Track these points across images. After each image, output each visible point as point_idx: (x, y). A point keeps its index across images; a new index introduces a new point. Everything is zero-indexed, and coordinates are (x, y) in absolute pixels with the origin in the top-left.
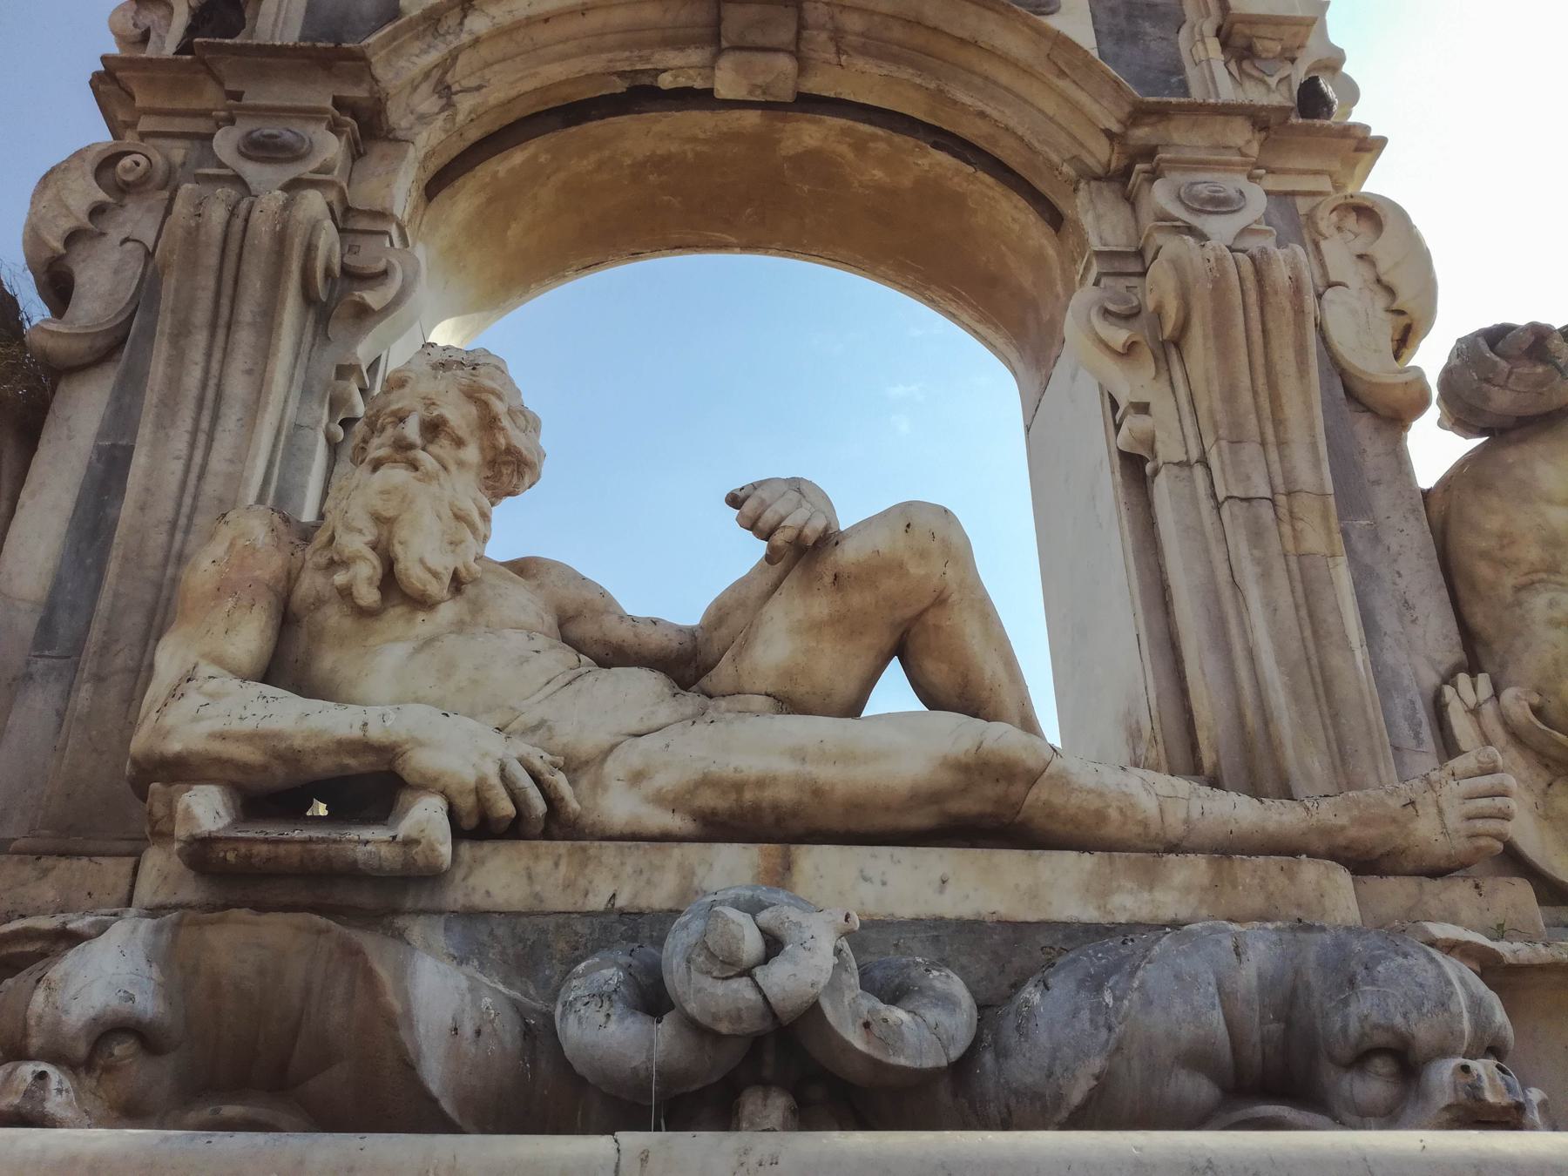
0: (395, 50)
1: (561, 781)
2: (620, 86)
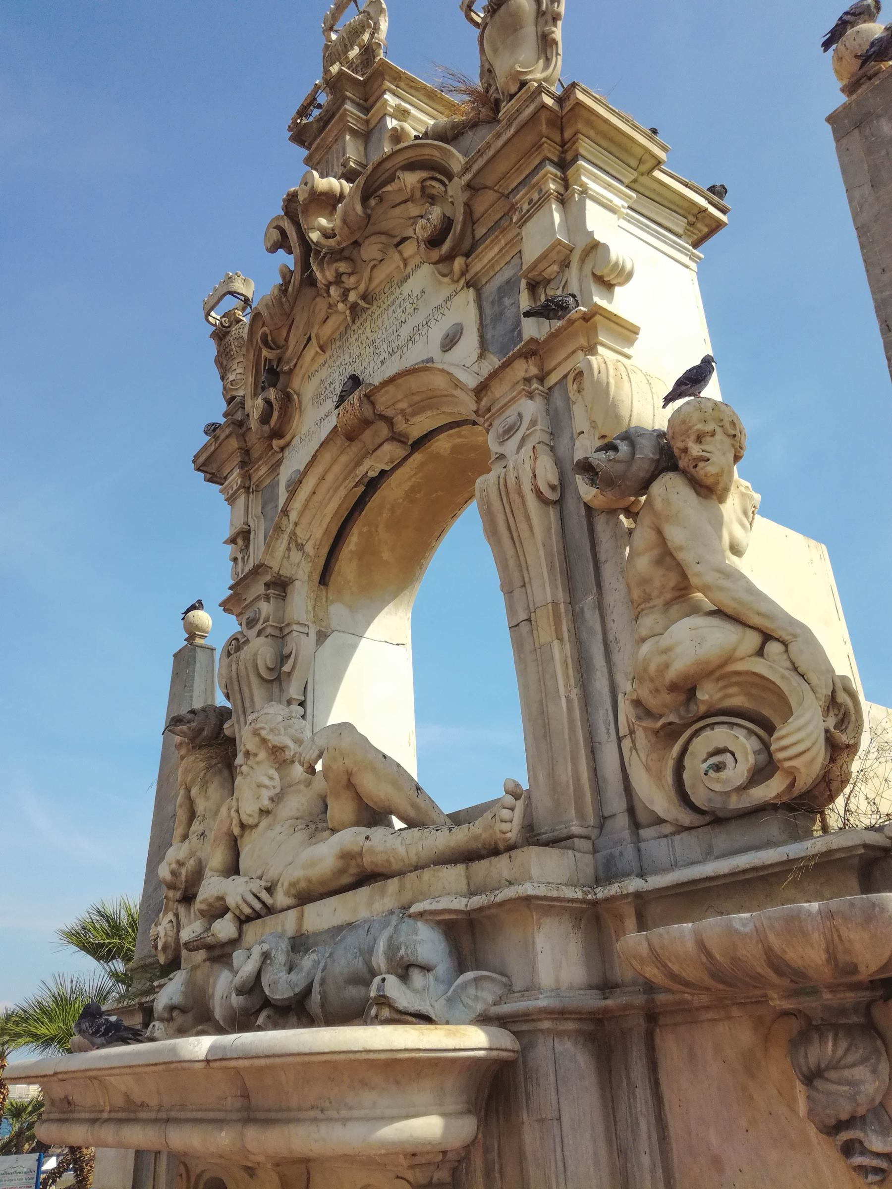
0: (272, 551)
1: (264, 895)
2: (362, 488)
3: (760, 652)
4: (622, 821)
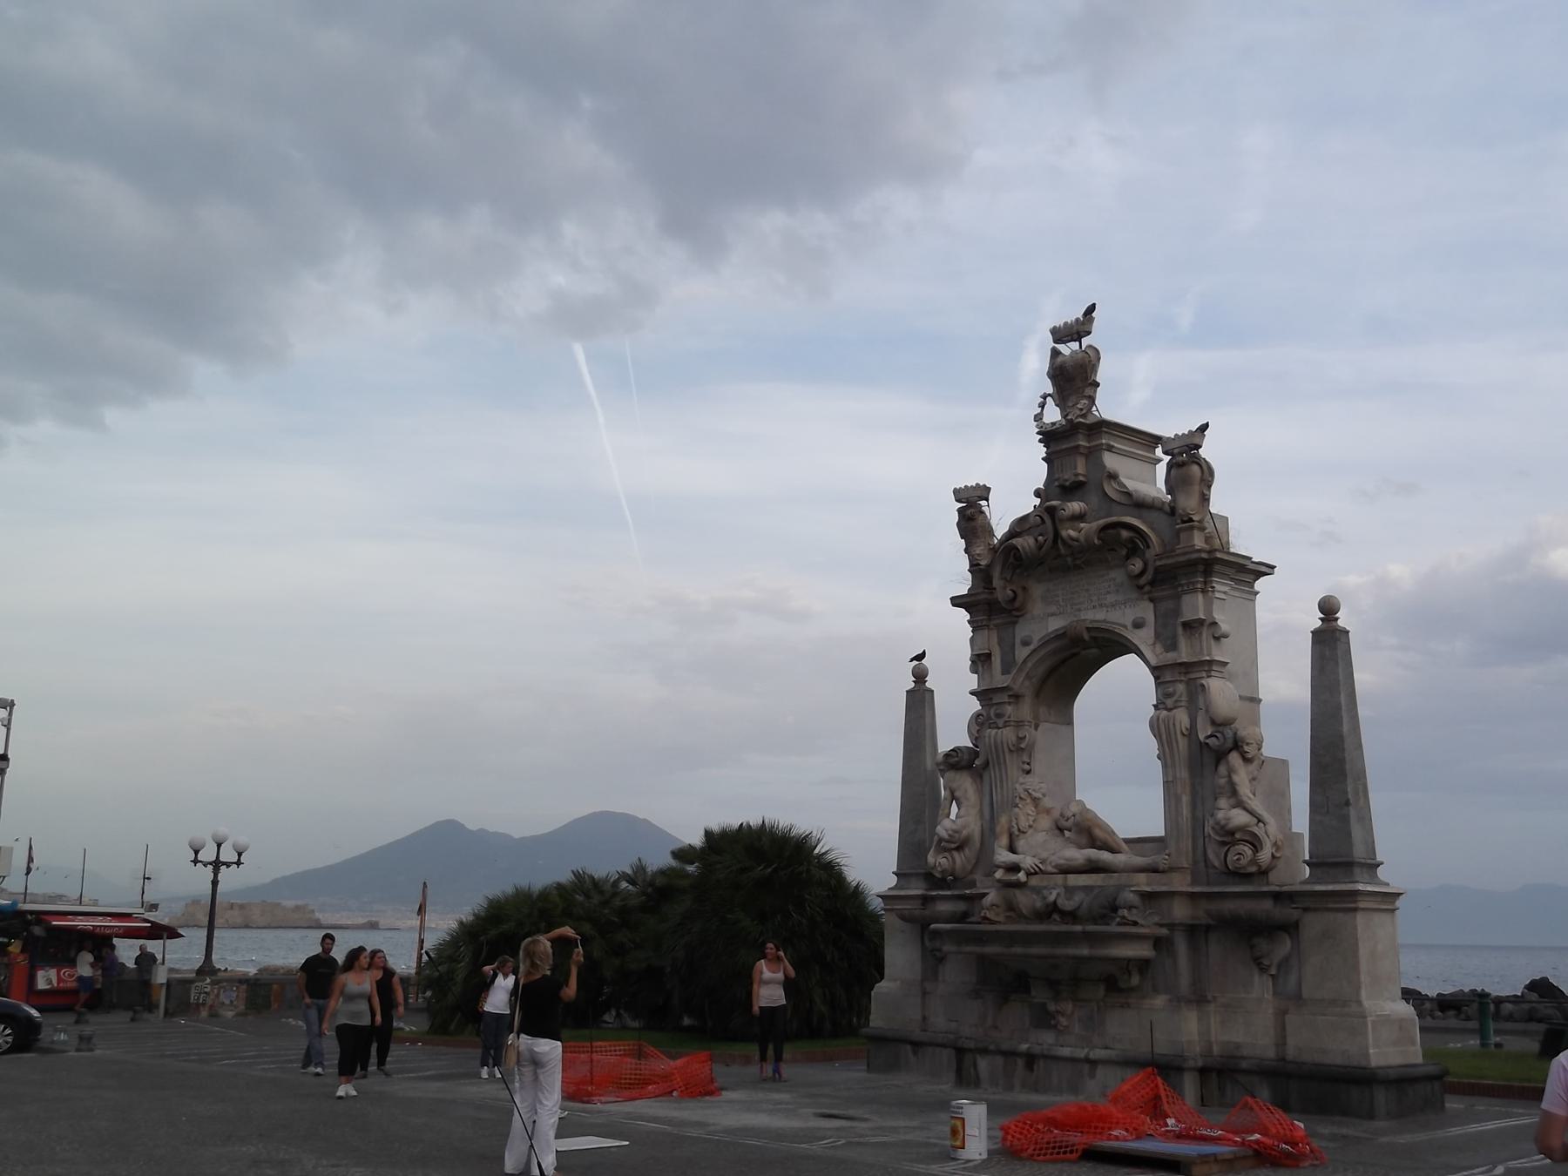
1: (1040, 865)
3: (1257, 825)
4: (1202, 864)
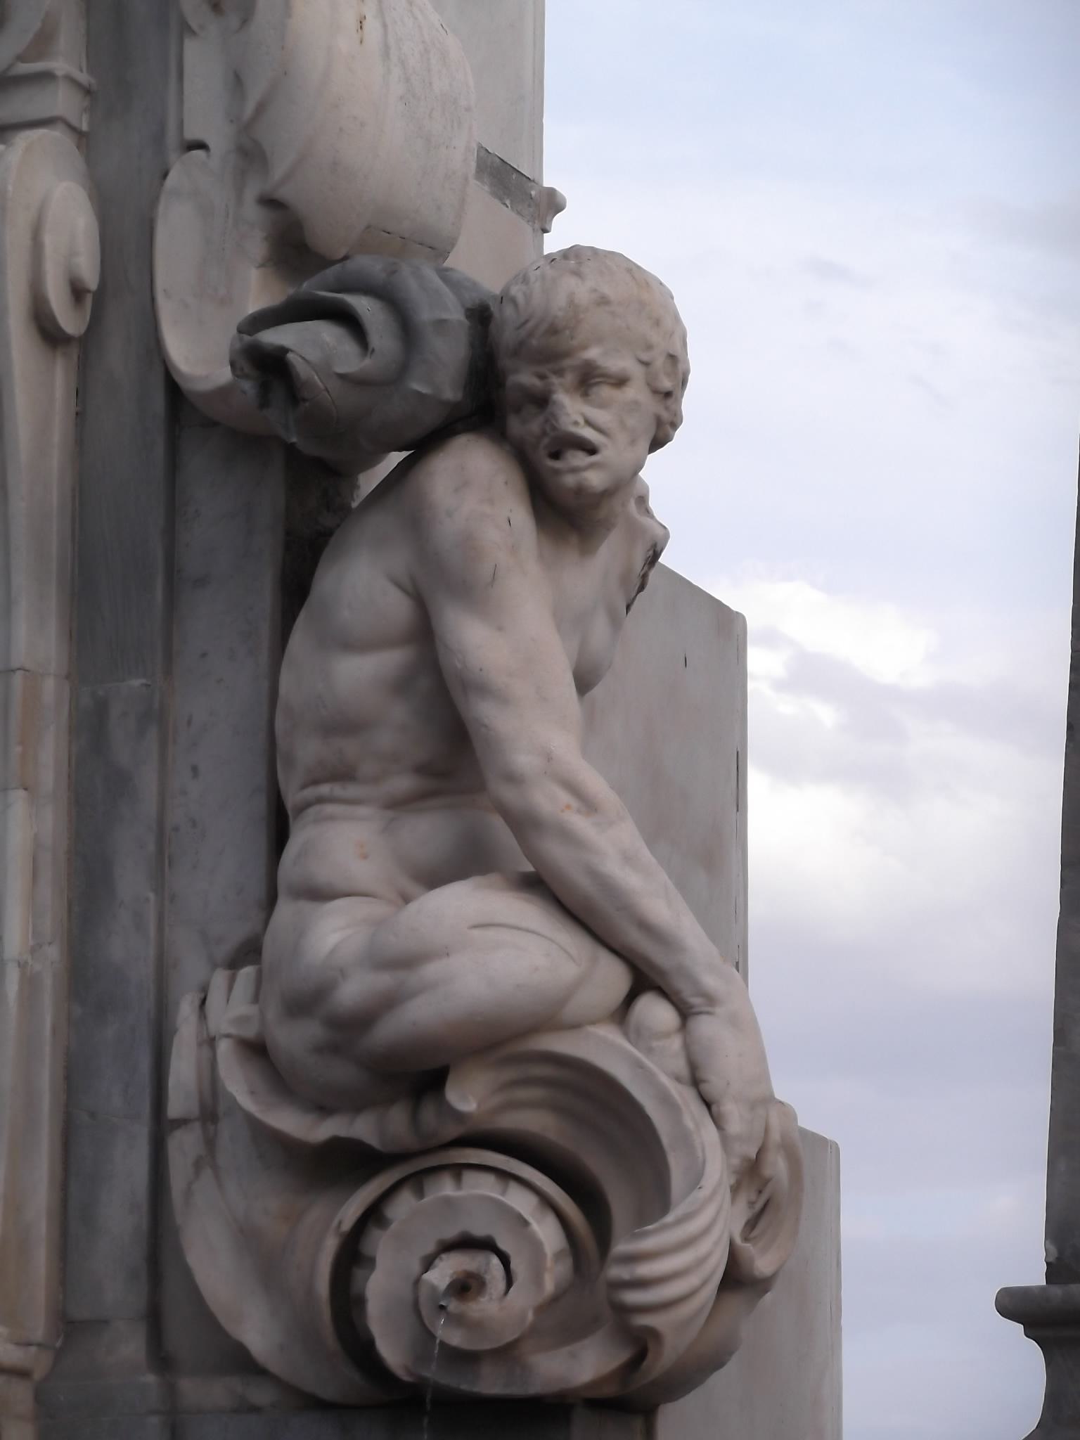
3: (622, 1012)
